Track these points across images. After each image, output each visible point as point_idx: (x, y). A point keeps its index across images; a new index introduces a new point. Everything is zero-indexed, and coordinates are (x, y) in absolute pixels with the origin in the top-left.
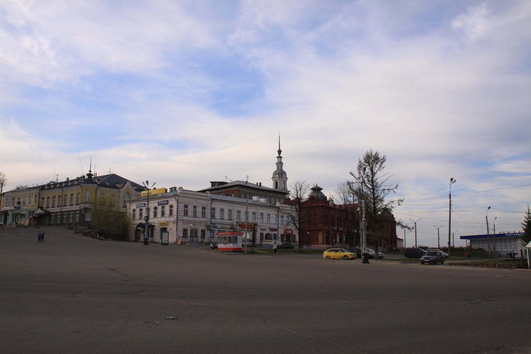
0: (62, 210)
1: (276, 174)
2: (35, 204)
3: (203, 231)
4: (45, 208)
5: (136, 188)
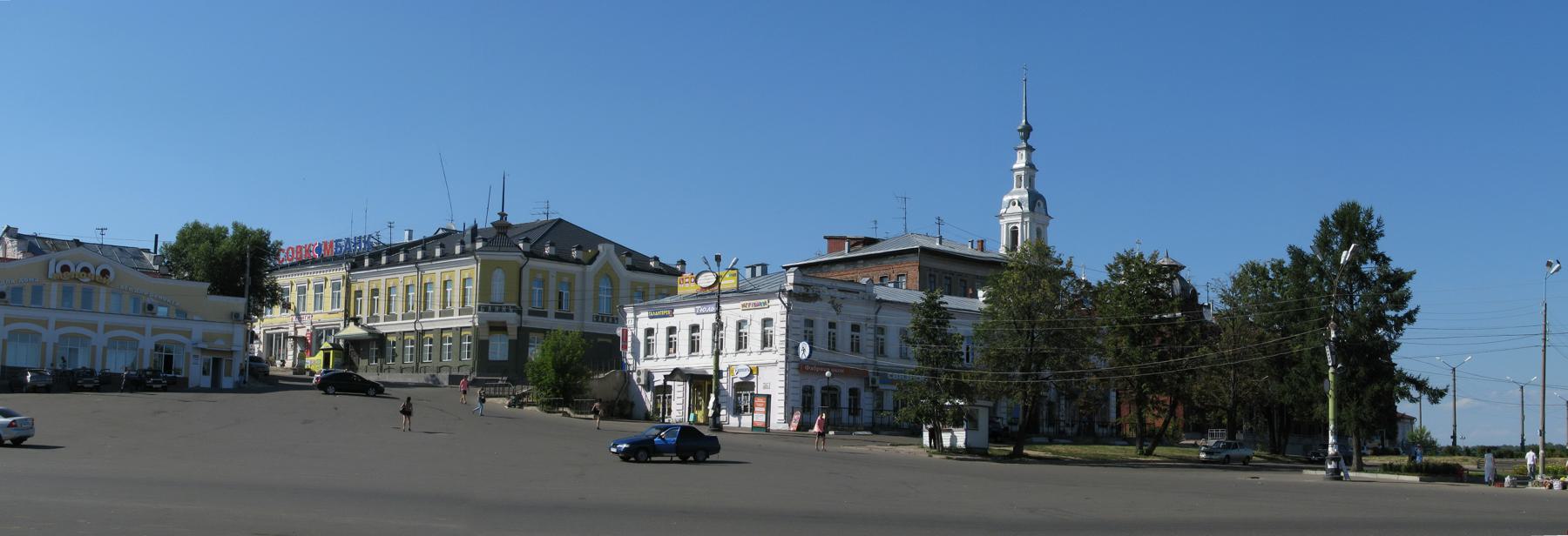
0: (419, 328)
1: (1014, 204)
2: (337, 310)
3: (854, 392)
4: (364, 322)
5: (629, 261)
